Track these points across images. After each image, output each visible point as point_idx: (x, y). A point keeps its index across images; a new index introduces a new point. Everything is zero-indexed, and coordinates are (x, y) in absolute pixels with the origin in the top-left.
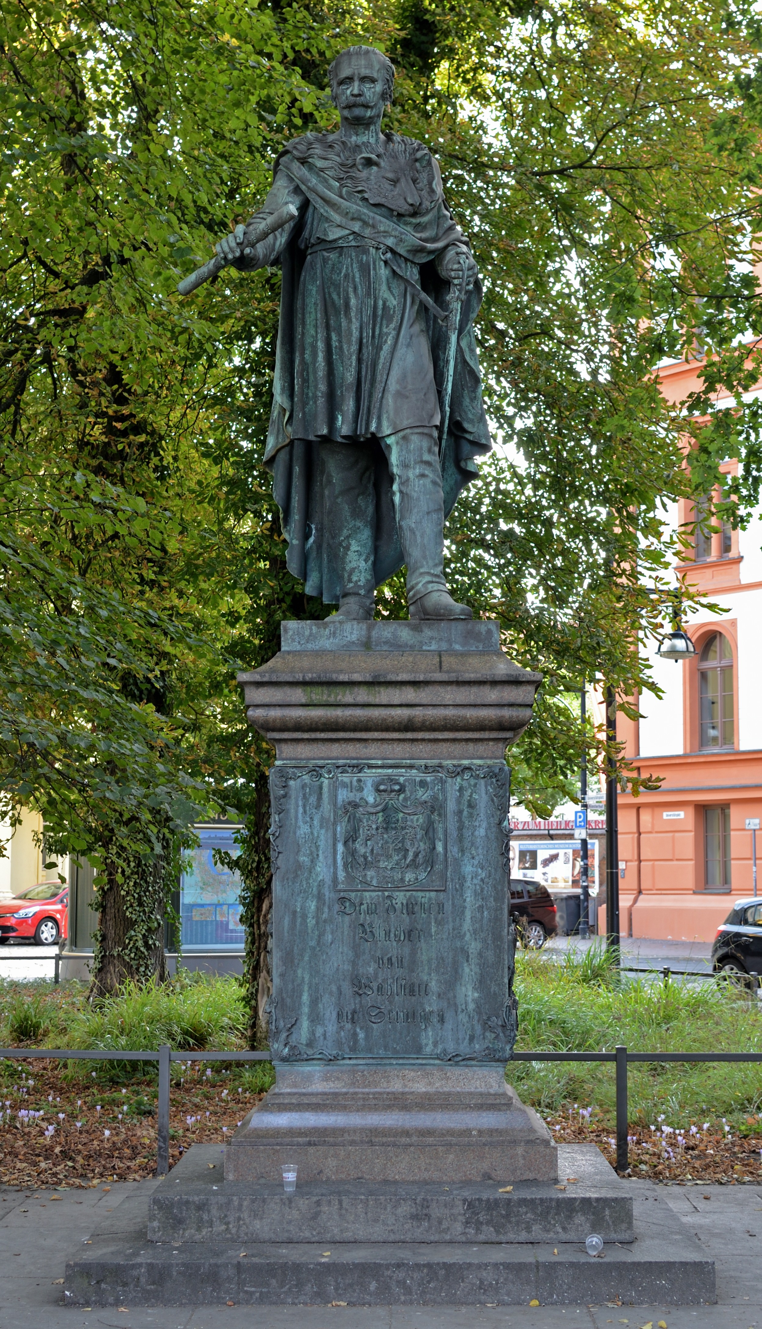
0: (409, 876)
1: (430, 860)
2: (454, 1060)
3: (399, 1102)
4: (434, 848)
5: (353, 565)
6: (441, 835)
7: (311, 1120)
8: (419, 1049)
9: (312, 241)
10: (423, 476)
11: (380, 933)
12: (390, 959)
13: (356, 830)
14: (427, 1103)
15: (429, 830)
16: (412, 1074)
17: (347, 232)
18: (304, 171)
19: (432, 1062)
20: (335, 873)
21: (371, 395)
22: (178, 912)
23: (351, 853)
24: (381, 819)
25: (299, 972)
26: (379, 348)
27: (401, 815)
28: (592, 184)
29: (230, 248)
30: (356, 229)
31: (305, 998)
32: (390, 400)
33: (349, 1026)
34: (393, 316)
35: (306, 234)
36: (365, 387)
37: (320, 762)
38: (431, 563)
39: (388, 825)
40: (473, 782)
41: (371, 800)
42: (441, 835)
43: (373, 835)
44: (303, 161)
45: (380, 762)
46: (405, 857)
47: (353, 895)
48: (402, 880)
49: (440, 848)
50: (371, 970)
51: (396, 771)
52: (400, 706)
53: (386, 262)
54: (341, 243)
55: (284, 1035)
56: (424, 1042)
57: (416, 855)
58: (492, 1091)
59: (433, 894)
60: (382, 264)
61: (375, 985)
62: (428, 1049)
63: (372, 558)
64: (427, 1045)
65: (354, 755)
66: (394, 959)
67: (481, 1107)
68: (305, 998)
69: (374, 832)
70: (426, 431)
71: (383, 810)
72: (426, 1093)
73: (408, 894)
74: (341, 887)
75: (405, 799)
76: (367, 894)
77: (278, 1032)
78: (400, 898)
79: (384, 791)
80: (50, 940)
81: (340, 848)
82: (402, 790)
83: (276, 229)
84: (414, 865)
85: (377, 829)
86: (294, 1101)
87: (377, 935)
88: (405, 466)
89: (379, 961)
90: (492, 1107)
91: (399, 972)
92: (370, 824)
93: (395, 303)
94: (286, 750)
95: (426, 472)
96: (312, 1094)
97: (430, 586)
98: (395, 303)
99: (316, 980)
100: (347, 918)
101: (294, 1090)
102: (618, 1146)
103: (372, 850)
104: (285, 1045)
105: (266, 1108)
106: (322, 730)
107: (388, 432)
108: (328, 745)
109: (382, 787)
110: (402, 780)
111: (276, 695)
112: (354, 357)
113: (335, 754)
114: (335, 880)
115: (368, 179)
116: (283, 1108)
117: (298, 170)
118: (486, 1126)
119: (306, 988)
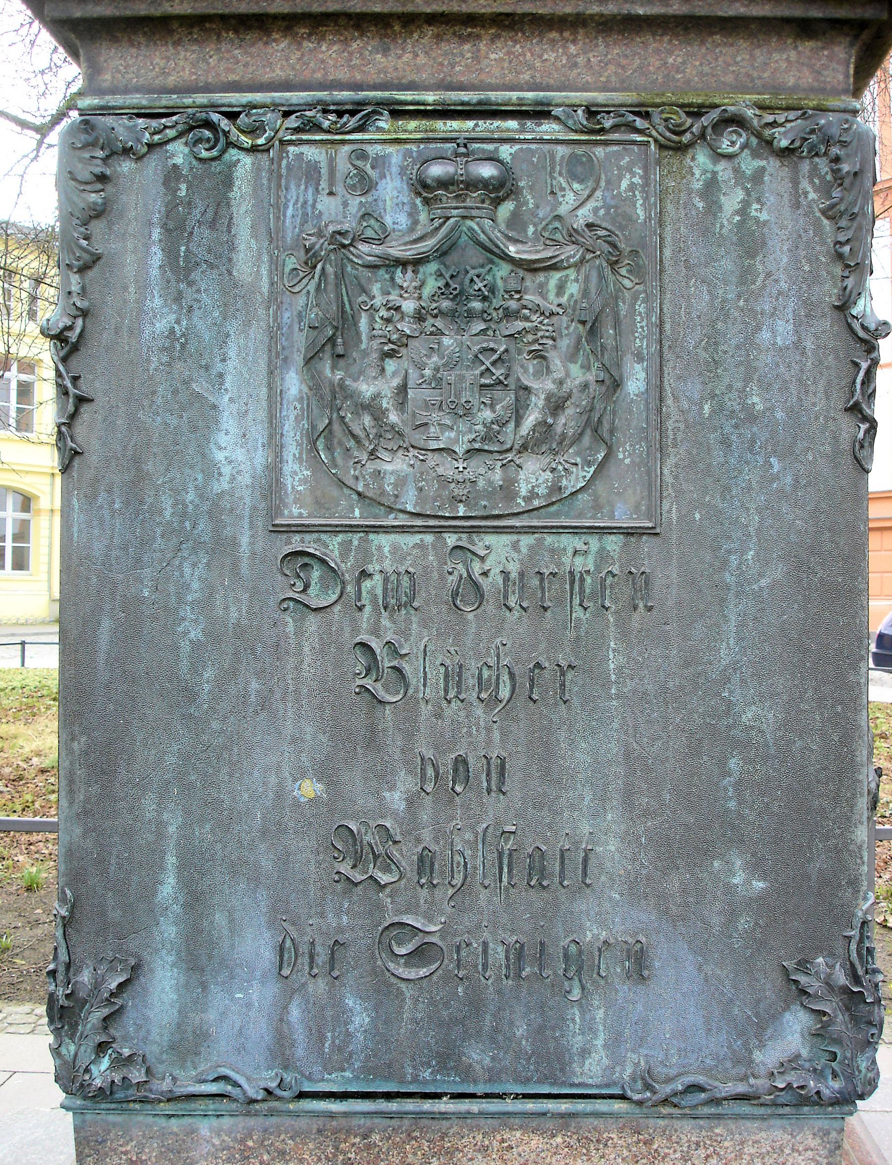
0: (533, 475)
4: (617, 384)
13: (344, 322)
16: (536, 1142)
20: (274, 470)
23: (331, 400)
24: (432, 285)
25: (149, 804)
28: (821, 1033)
31: (168, 888)
39: (459, 302)
41: (396, 219)
43: (405, 340)
47: (335, 542)
48: (508, 490)
49: (636, 381)
51: (484, 126)
56: (578, 1041)
57: (556, 405)
59: (613, 543)
61: (406, 855)
64: (585, 1052)
65: (342, 75)
68: (168, 888)
69: (406, 327)
73: (526, 541)
74: (295, 512)
76: (384, 541)
79: (444, 184)
81: (294, 384)
83: (72, 912)
84: (542, 440)
99: (205, 832)
103: (403, 389)
104: (101, 1048)
109: (436, 170)
110: (506, 151)
113: (278, 73)
114: (272, 486)
119: (171, 860)
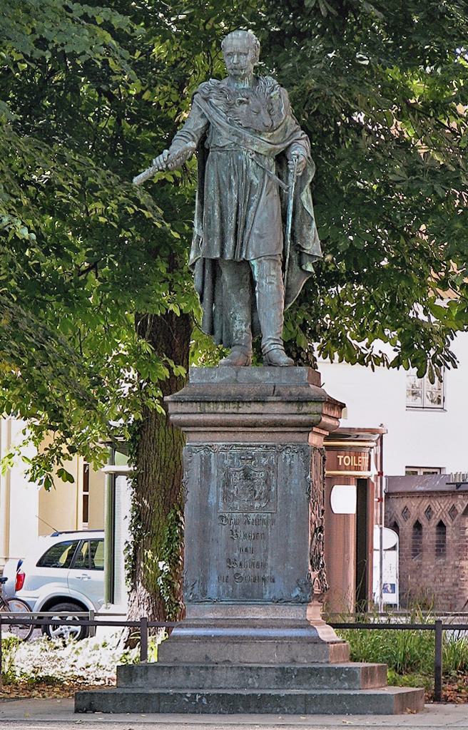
0: (257, 505)
1: (267, 497)
2: (278, 601)
3: (251, 624)
4: (270, 490)
5: (238, 328)
9: (212, 145)
11: (241, 535)
12: (246, 549)
14: (266, 625)
15: (267, 481)
21: (243, 237)
24: (242, 474)
27: (253, 472)
30: (235, 141)
32: (253, 241)
35: (208, 141)
36: (240, 231)
37: (209, 444)
38: (274, 333)
40: (291, 454)
42: (274, 483)
44: (206, 100)
45: (242, 444)
50: (236, 554)
52: (251, 414)
53: (253, 160)
54: (226, 148)
55: (190, 588)
58: (300, 618)
60: (250, 160)
63: (250, 324)
64: (265, 594)
66: (248, 549)
67: (292, 627)
70: (274, 258)
72: (265, 619)
75: (255, 464)
77: (187, 586)
80: (99, 23)
84: (259, 499)
89: (241, 550)
90: (301, 627)
92: (237, 478)
93: (258, 182)
94: (192, 437)
96: (206, 619)
97: (272, 346)
98: (258, 182)
100: (224, 527)
101: (196, 617)
102: (436, 685)
105: (181, 626)
107: (252, 258)
109: (243, 457)
111: (186, 408)
112: (233, 215)
116: (188, 626)
117: (205, 106)
118: (294, 635)
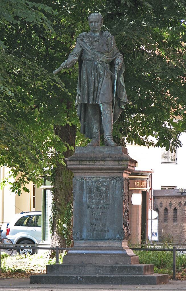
0: (102, 201)
1: (106, 198)
4: (107, 195)
6: (109, 192)
7: (84, 252)
8: (104, 237)
10: (107, 113)
11: (96, 213)
12: (98, 219)
14: (106, 249)
15: (106, 192)
17: (92, 57)
18: (82, 43)
19: (107, 240)
22: (34, 242)
26: (99, 84)
29: (64, 66)
32: (101, 96)
33: (89, 233)
34: (102, 76)
42: (109, 192)
44: (82, 40)
46: (101, 197)
50: (94, 221)
52: (100, 165)
53: (100, 64)
54: (90, 60)
57: (103, 197)
58: (119, 246)
61: (95, 224)
62: (106, 238)
65: (91, 175)
66: (99, 219)
71: (97, 187)
75: (101, 185)
78: (100, 206)
79: (97, 183)
82: (101, 183)
84: (103, 199)
85: (95, 191)
86: (77, 248)
87: (95, 213)
88: (104, 111)
91: (100, 221)
92: (94, 191)
93: (102, 73)
94: (76, 174)
95: (108, 112)
96: (82, 247)
97: (108, 138)
100: (89, 210)
101: (78, 246)
106: (84, 170)
108: (85, 173)
109: (96, 182)
115: (96, 45)
116: (75, 250)
